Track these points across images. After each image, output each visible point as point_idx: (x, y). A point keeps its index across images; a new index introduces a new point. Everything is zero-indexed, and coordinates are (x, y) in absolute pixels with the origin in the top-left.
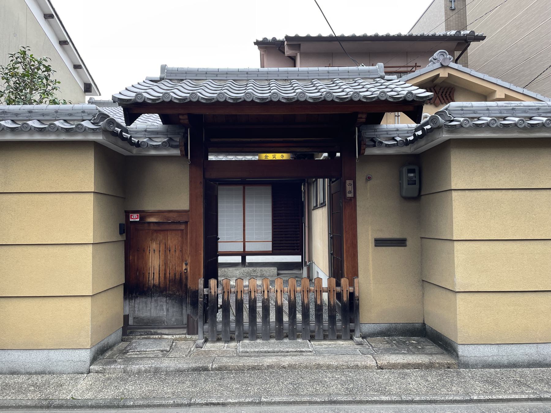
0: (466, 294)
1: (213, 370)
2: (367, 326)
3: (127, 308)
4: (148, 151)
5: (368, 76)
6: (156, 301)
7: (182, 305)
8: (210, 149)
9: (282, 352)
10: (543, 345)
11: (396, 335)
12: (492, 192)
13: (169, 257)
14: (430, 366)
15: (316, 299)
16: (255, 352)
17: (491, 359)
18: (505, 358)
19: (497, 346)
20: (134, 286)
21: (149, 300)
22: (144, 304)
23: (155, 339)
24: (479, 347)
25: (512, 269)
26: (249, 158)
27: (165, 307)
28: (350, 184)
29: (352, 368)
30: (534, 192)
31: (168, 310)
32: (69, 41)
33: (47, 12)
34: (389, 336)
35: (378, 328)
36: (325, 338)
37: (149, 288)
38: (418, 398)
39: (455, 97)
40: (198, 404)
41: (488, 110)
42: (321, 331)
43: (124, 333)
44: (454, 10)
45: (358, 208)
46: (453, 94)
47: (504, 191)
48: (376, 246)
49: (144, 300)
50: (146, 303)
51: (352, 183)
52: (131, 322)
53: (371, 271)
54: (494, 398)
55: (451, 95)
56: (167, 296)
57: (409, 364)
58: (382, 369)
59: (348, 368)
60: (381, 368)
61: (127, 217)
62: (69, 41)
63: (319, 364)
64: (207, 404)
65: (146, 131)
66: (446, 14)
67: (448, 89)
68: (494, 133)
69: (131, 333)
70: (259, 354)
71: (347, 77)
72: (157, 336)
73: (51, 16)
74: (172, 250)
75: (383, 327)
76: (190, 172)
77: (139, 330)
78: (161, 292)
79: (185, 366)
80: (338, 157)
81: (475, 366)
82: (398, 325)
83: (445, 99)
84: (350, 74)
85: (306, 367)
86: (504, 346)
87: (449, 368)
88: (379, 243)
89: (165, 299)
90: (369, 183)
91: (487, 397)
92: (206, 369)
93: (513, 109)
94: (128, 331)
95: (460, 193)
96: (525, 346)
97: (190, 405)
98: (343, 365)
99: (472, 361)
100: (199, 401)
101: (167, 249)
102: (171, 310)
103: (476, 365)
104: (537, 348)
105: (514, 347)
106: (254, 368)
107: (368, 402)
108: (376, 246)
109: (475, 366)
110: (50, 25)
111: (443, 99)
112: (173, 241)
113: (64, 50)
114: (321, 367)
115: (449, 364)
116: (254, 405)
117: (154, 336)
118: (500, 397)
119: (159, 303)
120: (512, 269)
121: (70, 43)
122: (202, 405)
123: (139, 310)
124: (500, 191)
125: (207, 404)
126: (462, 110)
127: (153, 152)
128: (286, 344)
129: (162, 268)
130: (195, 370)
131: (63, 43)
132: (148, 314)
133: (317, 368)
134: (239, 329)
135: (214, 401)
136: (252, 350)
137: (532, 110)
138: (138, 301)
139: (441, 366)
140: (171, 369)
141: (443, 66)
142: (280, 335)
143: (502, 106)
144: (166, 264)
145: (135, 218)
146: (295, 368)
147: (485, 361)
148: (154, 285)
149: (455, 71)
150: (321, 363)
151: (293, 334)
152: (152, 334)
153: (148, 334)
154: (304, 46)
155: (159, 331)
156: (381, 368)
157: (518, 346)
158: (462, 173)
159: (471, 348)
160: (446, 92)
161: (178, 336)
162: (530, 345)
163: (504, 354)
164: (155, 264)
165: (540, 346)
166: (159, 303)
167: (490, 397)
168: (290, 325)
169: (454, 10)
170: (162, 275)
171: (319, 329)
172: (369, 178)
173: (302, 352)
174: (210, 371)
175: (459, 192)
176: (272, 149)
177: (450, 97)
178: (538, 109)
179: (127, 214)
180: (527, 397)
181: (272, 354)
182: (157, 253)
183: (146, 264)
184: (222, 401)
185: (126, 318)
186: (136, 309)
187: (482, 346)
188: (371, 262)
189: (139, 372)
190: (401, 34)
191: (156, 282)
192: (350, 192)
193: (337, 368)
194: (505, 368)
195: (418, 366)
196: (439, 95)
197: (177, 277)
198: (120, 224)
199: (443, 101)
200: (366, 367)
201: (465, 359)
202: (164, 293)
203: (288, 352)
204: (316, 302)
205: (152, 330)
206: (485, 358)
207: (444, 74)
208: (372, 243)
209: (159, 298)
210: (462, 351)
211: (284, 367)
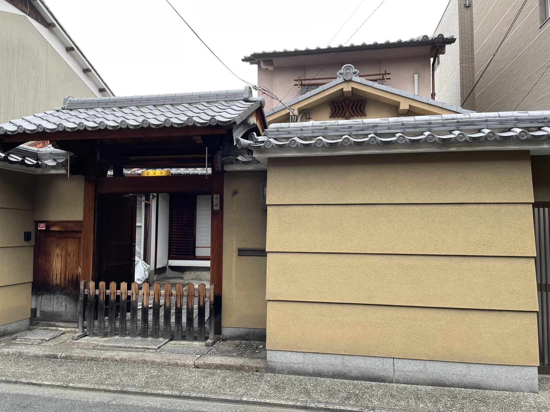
0: (276, 303)
1: (61, 358)
2: (228, 329)
3: (34, 303)
4: (50, 171)
5: (234, 99)
6: (57, 298)
7: (77, 303)
8: (124, 166)
9: (132, 348)
10: (349, 357)
11: (254, 340)
12: (304, 207)
13: (68, 261)
14: (240, 368)
15: (176, 302)
16: (110, 346)
17: (296, 366)
18: (310, 366)
19: (303, 354)
20: (41, 285)
21: (52, 296)
22: (48, 301)
23: (52, 330)
24: (286, 353)
25: (319, 281)
26: (182, 171)
27: (64, 304)
28: (217, 198)
29: (173, 365)
30: (344, 208)
31: (66, 306)
32: (91, 68)
33: (68, 46)
34: (247, 340)
35: (237, 332)
36: (184, 338)
37: (53, 287)
38: (194, 395)
39: (366, 109)
40: (22, 383)
41: (302, 130)
42: (180, 331)
43: (31, 324)
44: (469, 7)
45: (225, 220)
46: (364, 107)
47: (315, 206)
48: (239, 255)
49: (48, 296)
50: (50, 300)
51: (219, 197)
52: (38, 315)
53: (234, 278)
54: (262, 401)
55: (361, 108)
56: (65, 294)
57: (222, 365)
58: (198, 368)
59: (169, 365)
60: (197, 367)
61: (37, 227)
62: (91, 68)
63: (145, 360)
64: (28, 384)
65: (51, 153)
66: (460, 12)
67: (354, 102)
68: (299, 152)
69: (36, 324)
70: (113, 348)
71: (215, 100)
72: (54, 328)
73: (72, 49)
74: (71, 255)
75: (242, 331)
76: (85, 188)
77: (43, 322)
78: (62, 291)
79: (41, 353)
80: (110, 178)
81: (281, 371)
82: (256, 330)
83: (355, 111)
84: (218, 97)
85: (134, 362)
86: (310, 354)
87: (257, 371)
88: (242, 252)
89: (64, 297)
90: (236, 197)
91: (255, 400)
92: (55, 357)
93: (326, 129)
94: (34, 322)
95: (274, 207)
96: (330, 357)
97: (16, 383)
98: (164, 362)
99: (278, 366)
100: (24, 380)
101: (67, 254)
102: (68, 306)
103: (283, 370)
104: (343, 359)
105: (320, 357)
106: (92, 359)
107: (152, 394)
108: (239, 255)
109: (281, 371)
110: (73, 56)
111: (354, 112)
112: (72, 247)
113: (89, 77)
114: (147, 362)
115: (257, 367)
116: (62, 389)
117: (52, 328)
118: (268, 401)
119: (60, 300)
120: (319, 281)
121: (92, 70)
122: (24, 383)
123: (45, 305)
124: (311, 206)
125: (28, 384)
126: (278, 131)
127: (53, 172)
128: (139, 341)
129: (63, 270)
130: (49, 357)
131: (86, 71)
132: (51, 309)
133: (143, 363)
134: (111, 326)
135: (34, 382)
136: (108, 345)
137: (344, 128)
138: (44, 297)
139: (251, 369)
140: (31, 354)
141: (346, 81)
142: (144, 333)
143: (317, 126)
144: (66, 267)
145: (42, 227)
146: (125, 362)
147: (291, 367)
148: (56, 284)
149: (358, 84)
150: (147, 359)
151: (156, 334)
152: (51, 326)
153: (48, 326)
154: (276, 61)
155: (57, 324)
156: (197, 367)
157: (324, 355)
158: (279, 190)
159: (278, 354)
160: (357, 105)
161: (69, 329)
162: (335, 356)
163: (309, 362)
164: (57, 266)
165: (346, 357)
166: (60, 300)
167: (259, 400)
168: (153, 325)
169: (469, 7)
170: (63, 277)
171: (178, 330)
172: (235, 193)
173: (148, 349)
174: (58, 358)
175: (274, 207)
176: (184, 165)
177: (360, 110)
178: (350, 127)
179: (37, 223)
180: (293, 403)
181: (124, 349)
182: (59, 257)
183: (51, 266)
184: (40, 382)
185: (34, 311)
186: (43, 304)
187: (289, 353)
188: (234, 270)
189: (8, 354)
190: (426, 36)
191: (58, 282)
192: (217, 205)
193: (159, 364)
194: (309, 376)
195: (229, 368)
196: (350, 108)
197: (74, 278)
198: (25, 233)
199: (353, 114)
200: (184, 366)
201: (273, 364)
202: (64, 292)
203: (136, 348)
204: (176, 306)
205: (52, 323)
206: (292, 365)
207: (347, 88)
208: (235, 253)
209: (60, 296)
210: (274, 357)
211: (116, 361)
